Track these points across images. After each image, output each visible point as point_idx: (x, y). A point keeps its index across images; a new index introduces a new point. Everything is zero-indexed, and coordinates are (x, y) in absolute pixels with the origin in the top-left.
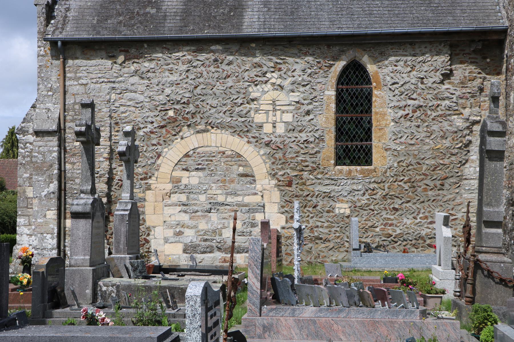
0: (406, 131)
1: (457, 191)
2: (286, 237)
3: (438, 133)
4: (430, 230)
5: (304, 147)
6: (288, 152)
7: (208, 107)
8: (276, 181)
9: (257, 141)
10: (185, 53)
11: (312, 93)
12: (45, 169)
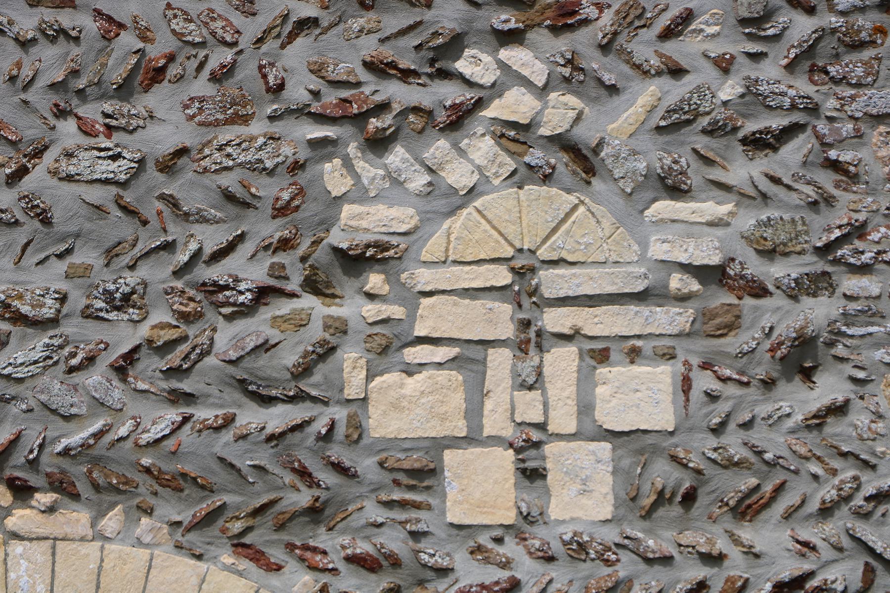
11: (829, 201)
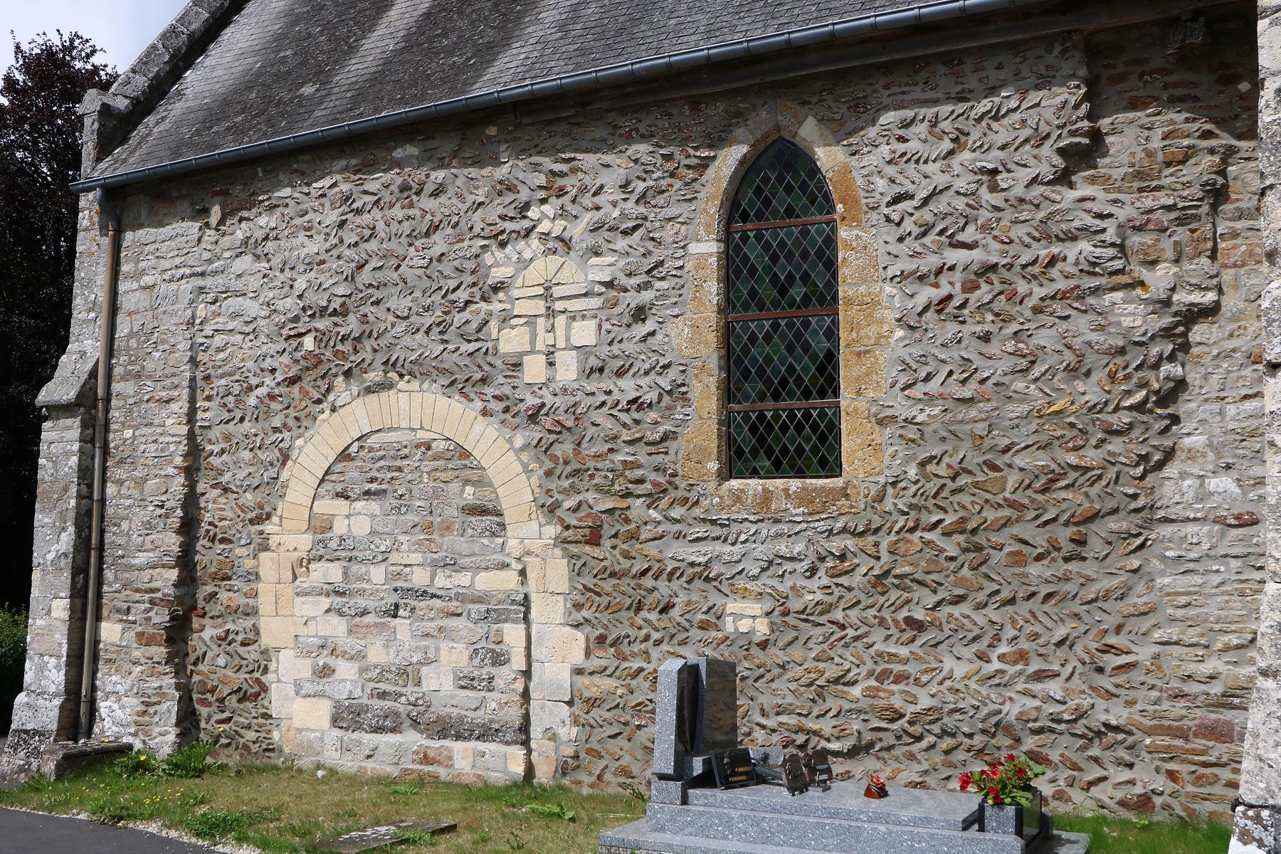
0: (943, 356)
1: (1135, 562)
2: (587, 701)
3: (1057, 357)
4: (1037, 703)
5: (629, 422)
6: (587, 438)
7: (391, 318)
8: (559, 528)
9: (508, 410)
10: (338, 177)
11: (650, 253)
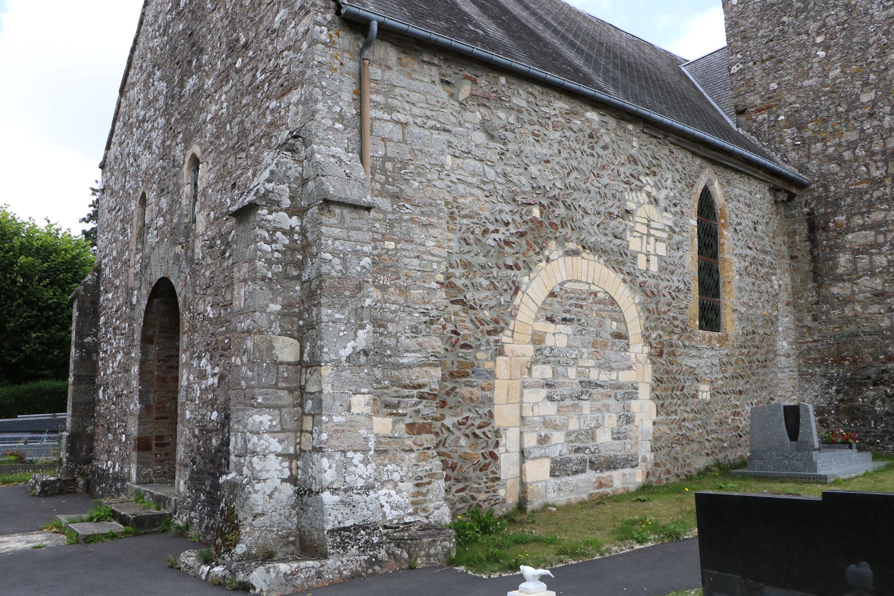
12: (347, 293)
